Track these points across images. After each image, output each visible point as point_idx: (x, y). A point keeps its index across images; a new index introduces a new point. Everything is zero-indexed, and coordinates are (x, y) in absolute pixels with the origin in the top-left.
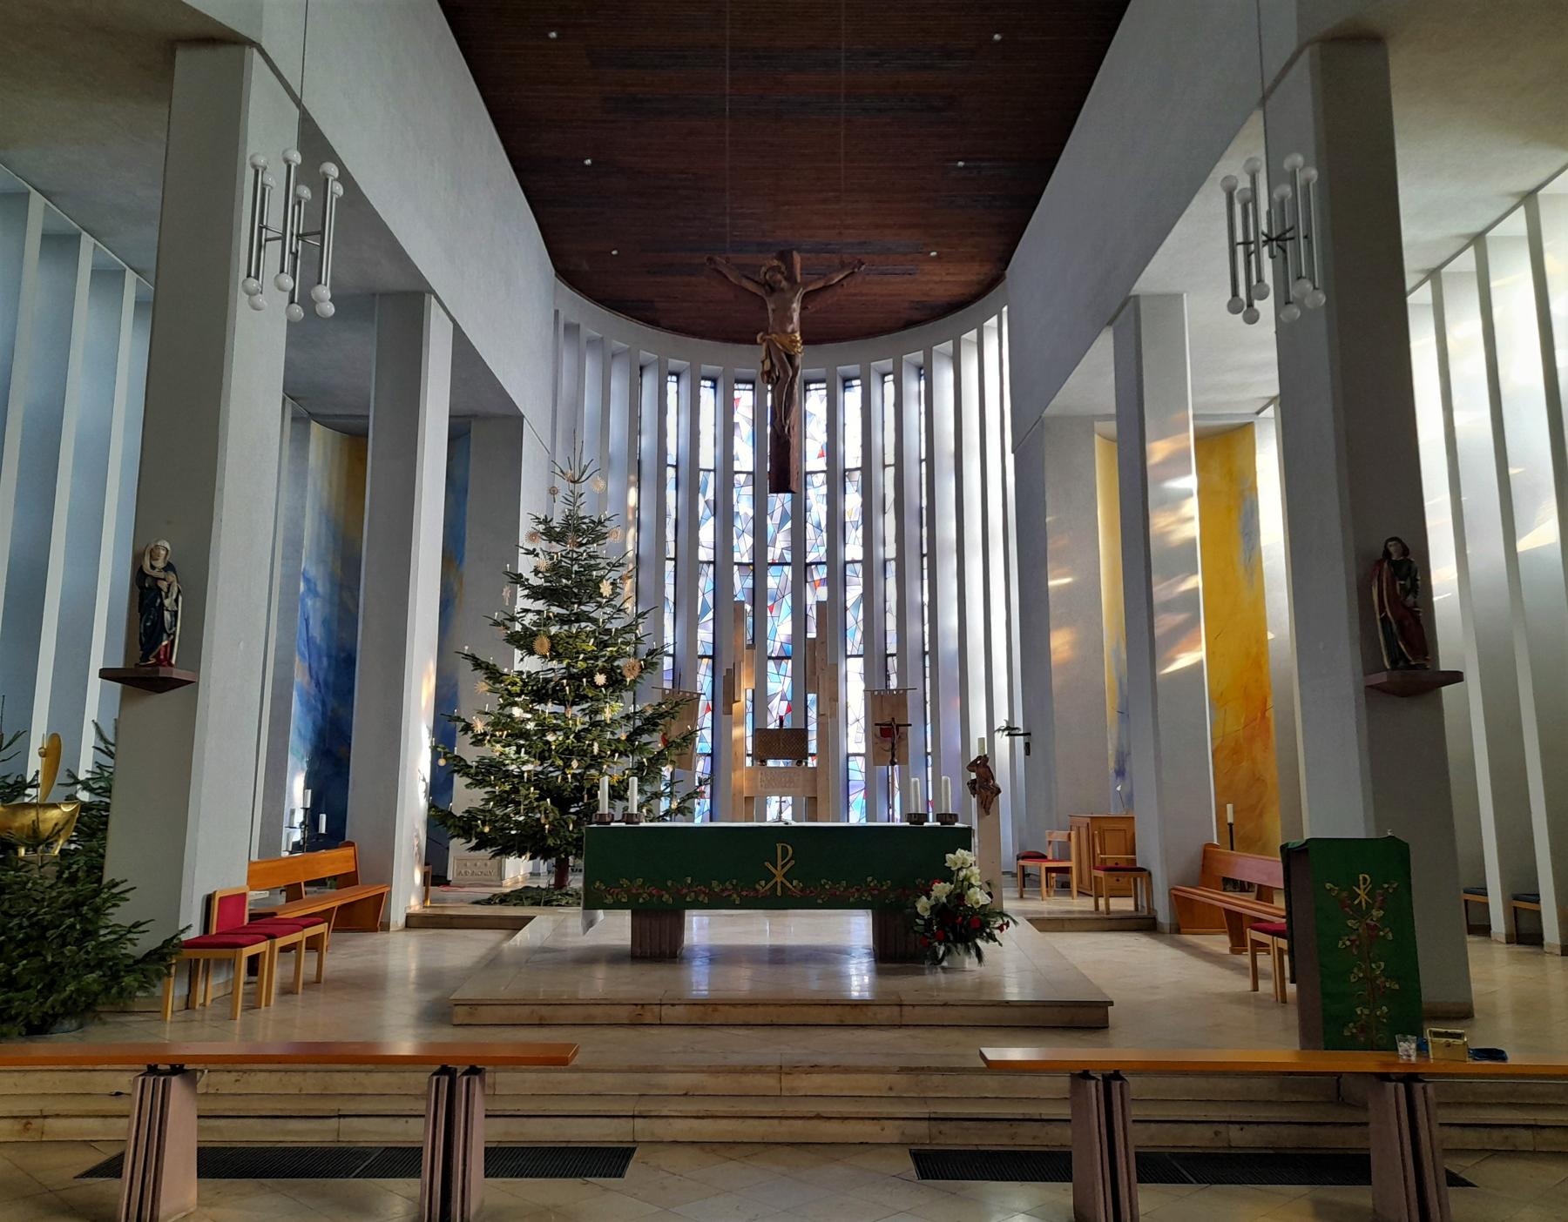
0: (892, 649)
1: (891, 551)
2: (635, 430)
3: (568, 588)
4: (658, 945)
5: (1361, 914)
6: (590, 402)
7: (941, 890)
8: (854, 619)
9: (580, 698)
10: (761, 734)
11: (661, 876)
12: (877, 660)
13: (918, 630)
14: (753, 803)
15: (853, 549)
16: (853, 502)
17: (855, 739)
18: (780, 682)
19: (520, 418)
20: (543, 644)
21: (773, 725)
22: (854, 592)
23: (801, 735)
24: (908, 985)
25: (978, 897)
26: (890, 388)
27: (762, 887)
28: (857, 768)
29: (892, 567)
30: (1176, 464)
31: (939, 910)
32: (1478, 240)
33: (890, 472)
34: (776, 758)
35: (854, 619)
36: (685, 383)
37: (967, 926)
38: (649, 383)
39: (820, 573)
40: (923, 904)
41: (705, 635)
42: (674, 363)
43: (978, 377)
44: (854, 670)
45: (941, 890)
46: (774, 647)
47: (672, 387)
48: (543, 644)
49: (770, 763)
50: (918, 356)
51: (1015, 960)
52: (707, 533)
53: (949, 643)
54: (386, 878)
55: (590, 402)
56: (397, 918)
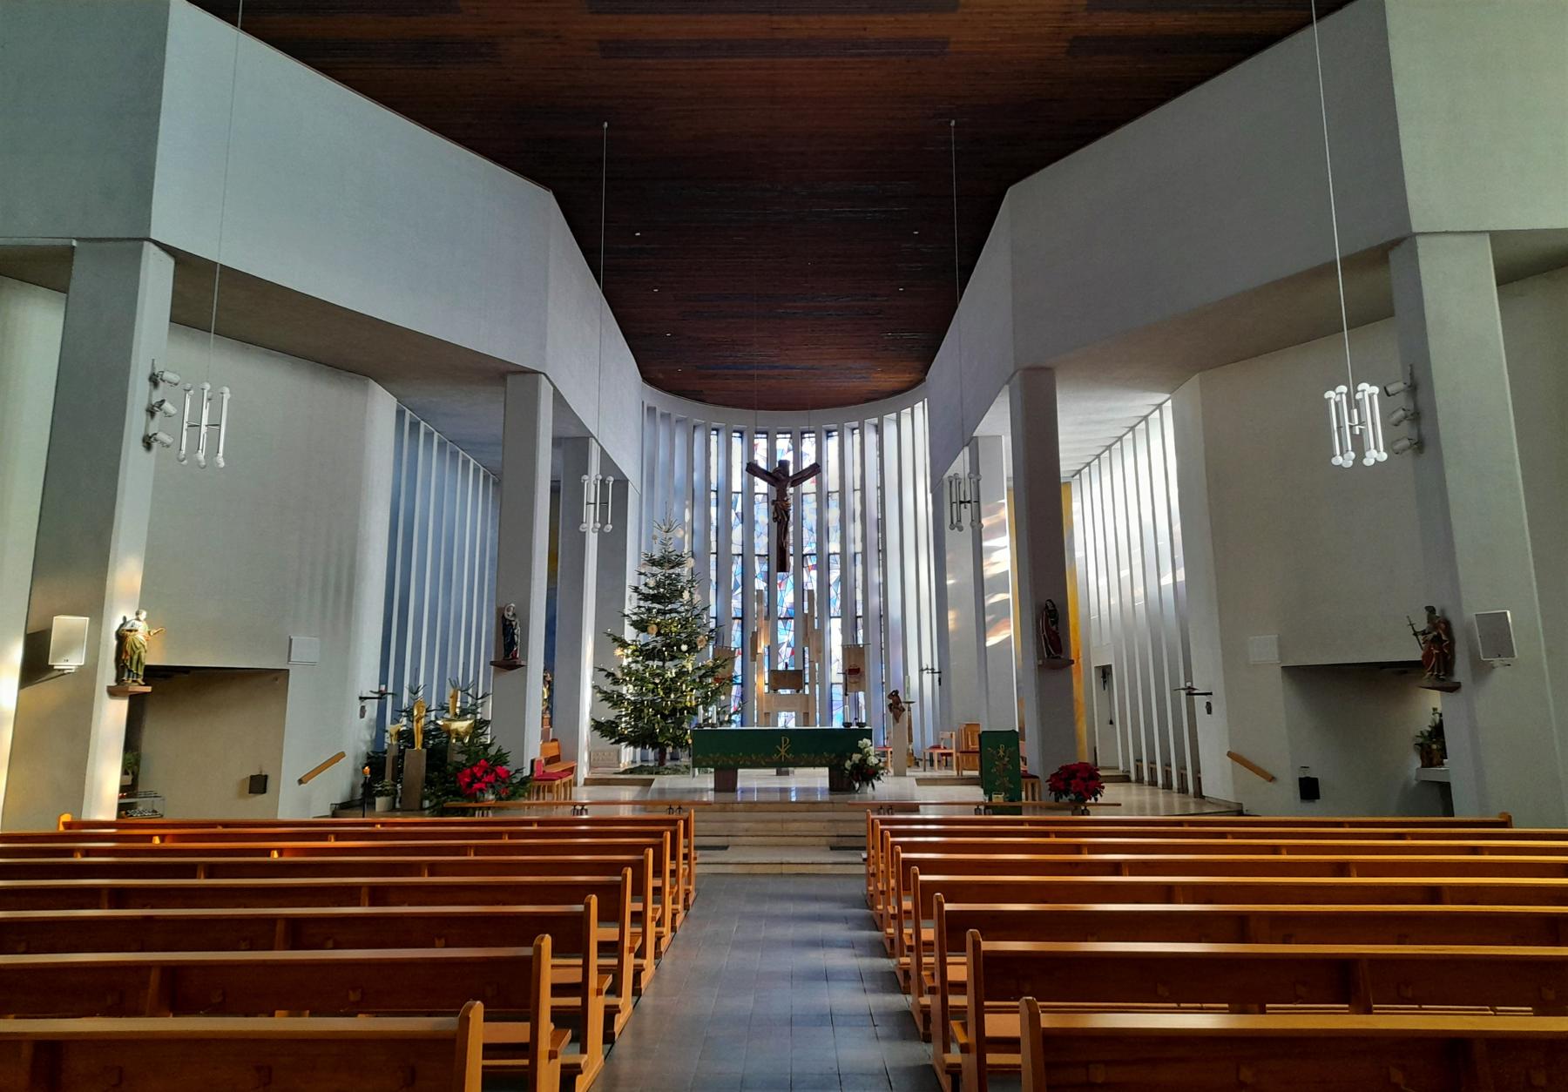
0: (860, 613)
1: (859, 548)
2: (690, 469)
3: (663, 594)
4: (726, 783)
5: (1001, 759)
6: (662, 454)
7: (856, 757)
8: (835, 592)
9: (673, 658)
10: (774, 673)
11: (728, 752)
12: (850, 622)
13: (875, 601)
14: (769, 715)
15: (834, 547)
16: (833, 514)
17: (836, 672)
18: (786, 635)
19: (627, 481)
20: (653, 629)
21: (781, 667)
22: (835, 574)
23: (799, 674)
24: (838, 797)
25: (873, 760)
26: (857, 437)
27: (775, 757)
28: (838, 691)
29: (859, 557)
30: (997, 530)
31: (854, 766)
32: (1145, 418)
33: (858, 494)
34: (784, 688)
35: (835, 592)
36: (722, 435)
37: (867, 774)
38: (699, 437)
39: (812, 561)
40: (848, 764)
41: (736, 603)
42: (715, 425)
43: (911, 429)
44: (835, 626)
45: (856, 757)
46: (781, 612)
47: (714, 438)
48: (653, 629)
49: (781, 691)
50: (876, 421)
51: (886, 787)
52: (737, 534)
53: (894, 611)
54: (576, 760)
55: (662, 454)
56: (581, 781)
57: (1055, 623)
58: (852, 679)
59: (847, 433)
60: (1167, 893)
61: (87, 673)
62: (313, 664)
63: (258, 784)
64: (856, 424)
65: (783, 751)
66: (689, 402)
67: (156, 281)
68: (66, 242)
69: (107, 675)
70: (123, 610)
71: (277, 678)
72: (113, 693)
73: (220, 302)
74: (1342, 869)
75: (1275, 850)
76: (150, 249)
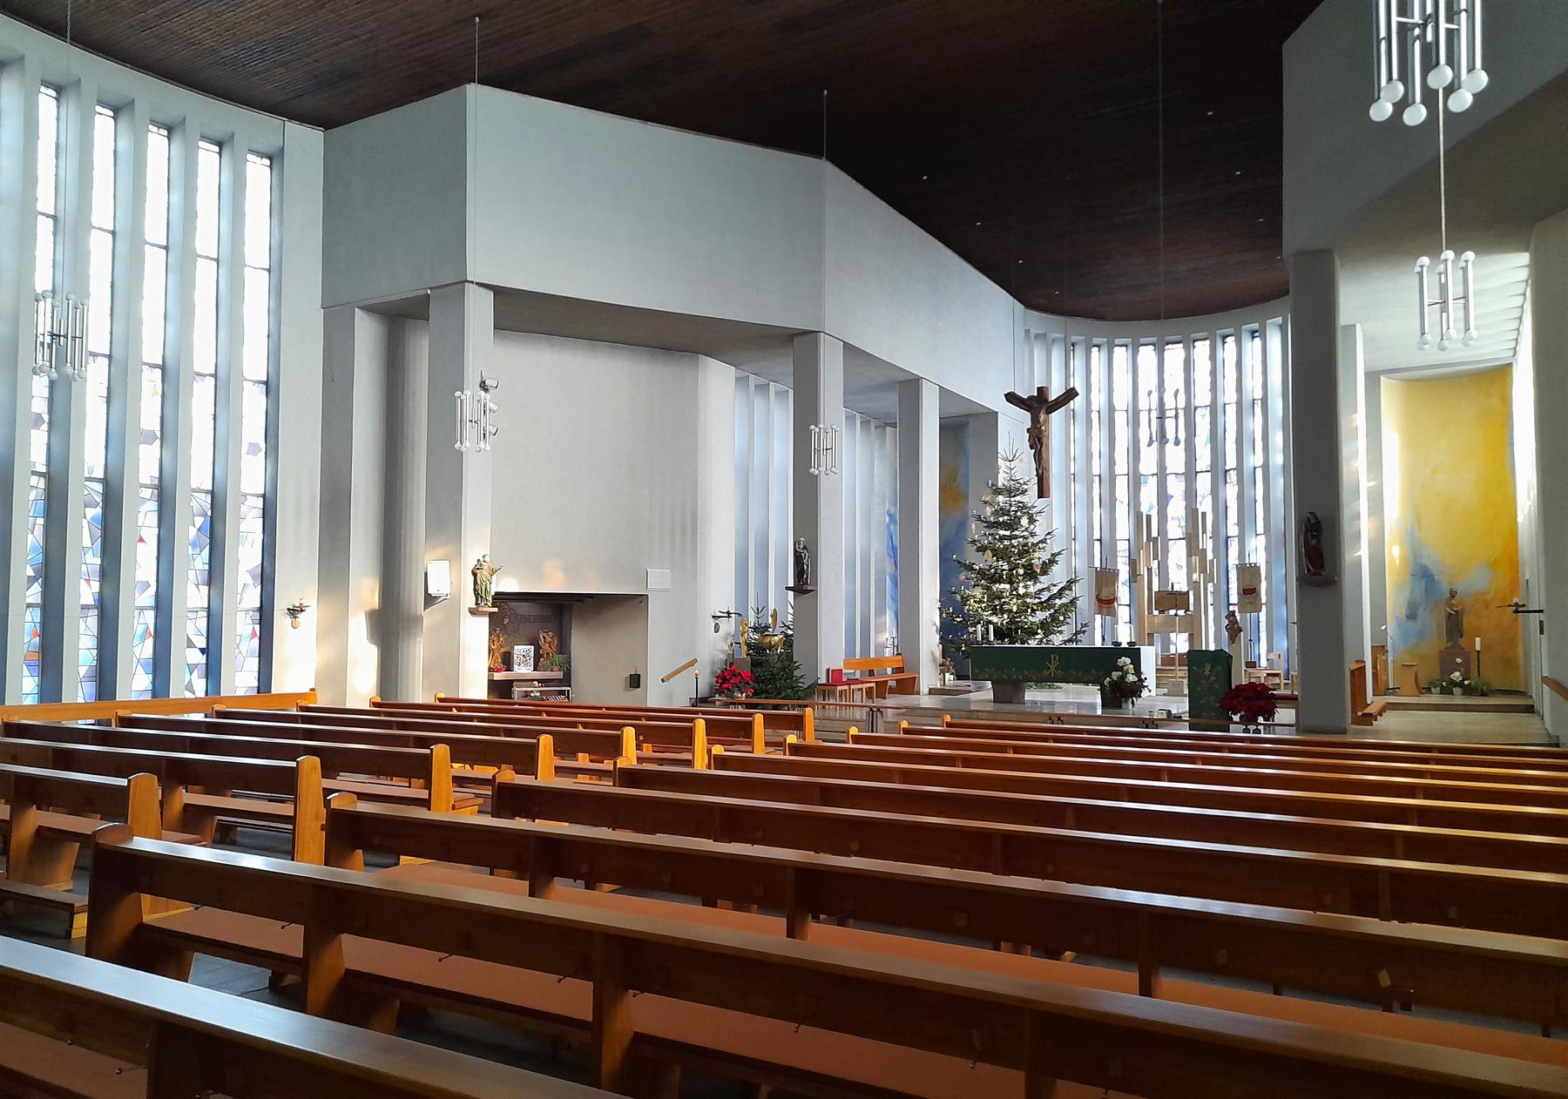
27: (1046, 673)
29: (1259, 472)
42: (1096, 340)
45: (1115, 675)
57: (1317, 537)
58: (1249, 598)
59: (1246, 339)
60: (886, 775)
61: (455, 601)
62: (665, 590)
63: (635, 681)
64: (1255, 326)
65: (1053, 668)
66: (1089, 321)
67: (479, 310)
68: (421, 293)
69: (470, 601)
70: (476, 549)
71: (642, 599)
72: (473, 612)
73: (524, 314)
74: (1155, 774)
75: (1004, 749)
76: (470, 288)
